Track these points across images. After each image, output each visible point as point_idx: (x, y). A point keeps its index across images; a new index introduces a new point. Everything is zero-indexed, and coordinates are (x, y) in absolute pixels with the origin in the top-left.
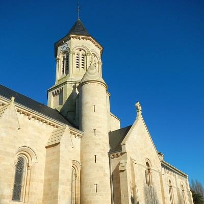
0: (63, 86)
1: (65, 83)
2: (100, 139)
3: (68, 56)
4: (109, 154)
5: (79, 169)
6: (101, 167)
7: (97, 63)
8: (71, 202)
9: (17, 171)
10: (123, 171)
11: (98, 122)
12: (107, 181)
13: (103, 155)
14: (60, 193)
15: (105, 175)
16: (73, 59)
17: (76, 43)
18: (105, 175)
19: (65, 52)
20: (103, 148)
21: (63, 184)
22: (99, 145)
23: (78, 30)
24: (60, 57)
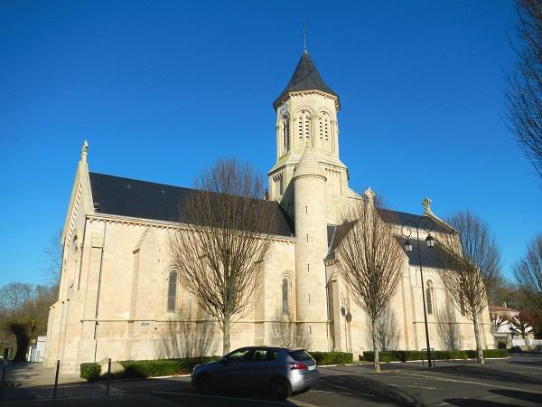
0: (283, 170)
1: (284, 167)
2: (314, 246)
3: (288, 123)
4: (325, 260)
5: (294, 277)
6: (315, 277)
7: (328, 123)
8: (266, 247)
9: (283, 291)
10: (334, 281)
11: (310, 226)
12: (324, 291)
13: (317, 263)
14: (266, 307)
15: (321, 285)
16: (294, 127)
17: (297, 102)
18: (321, 285)
19: (285, 117)
20: (316, 255)
21: (269, 298)
22: (312, 252)
23: (305, 78)
24: (281, 123)
